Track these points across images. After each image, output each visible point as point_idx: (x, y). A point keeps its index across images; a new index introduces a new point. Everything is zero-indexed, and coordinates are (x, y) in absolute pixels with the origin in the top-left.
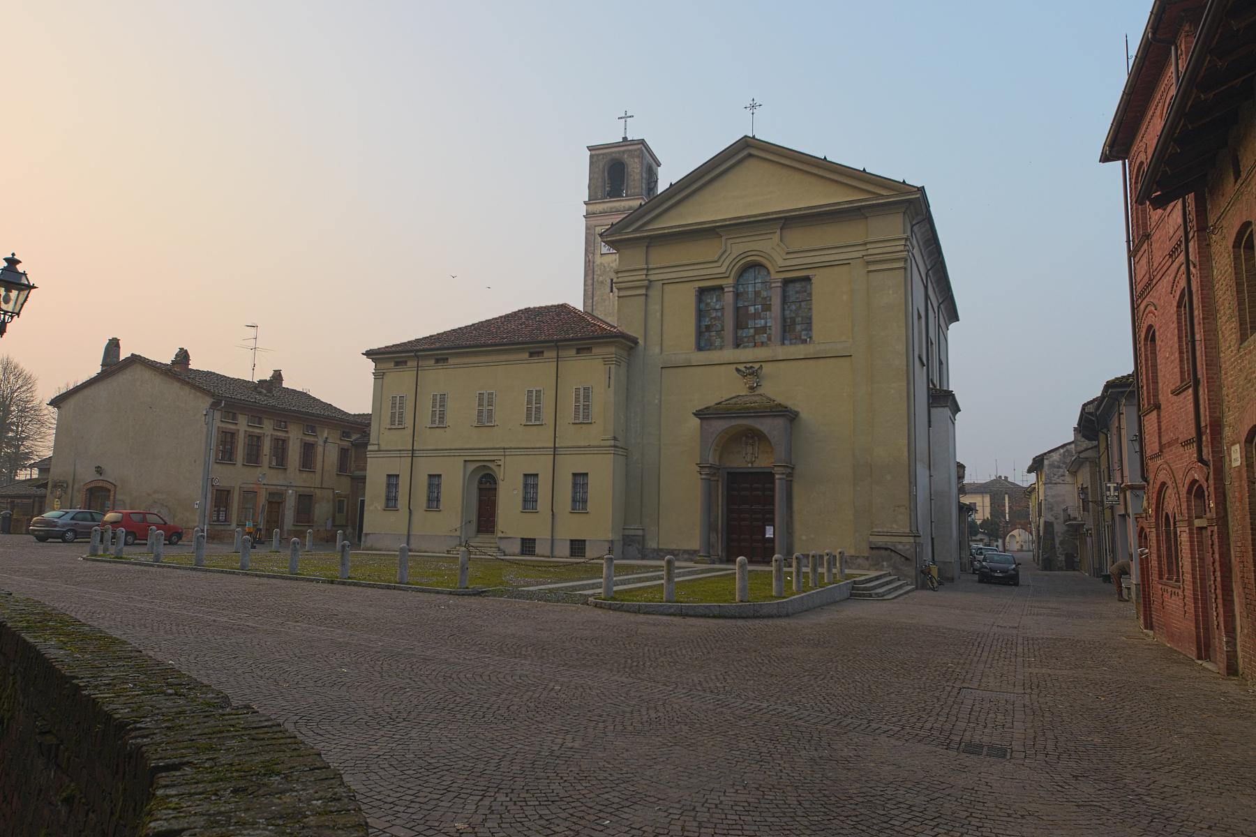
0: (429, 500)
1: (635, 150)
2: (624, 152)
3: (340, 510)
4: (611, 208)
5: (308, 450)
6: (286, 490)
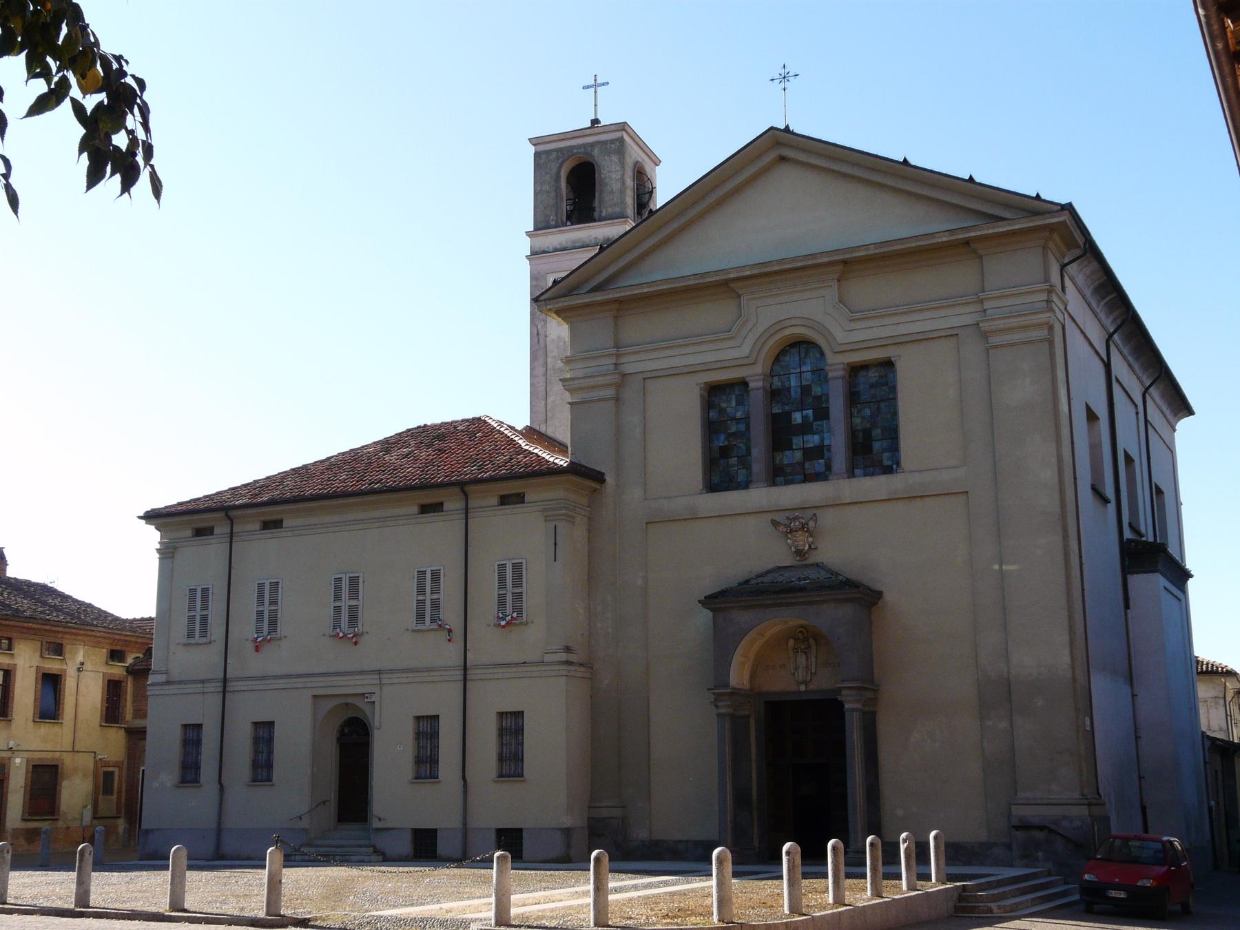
0: (255, 765)
1: (612, 141)
2: (592, 145)
3: (107, 789)
4: (574, 242)
5: (51, 682)
6: (9, 759)
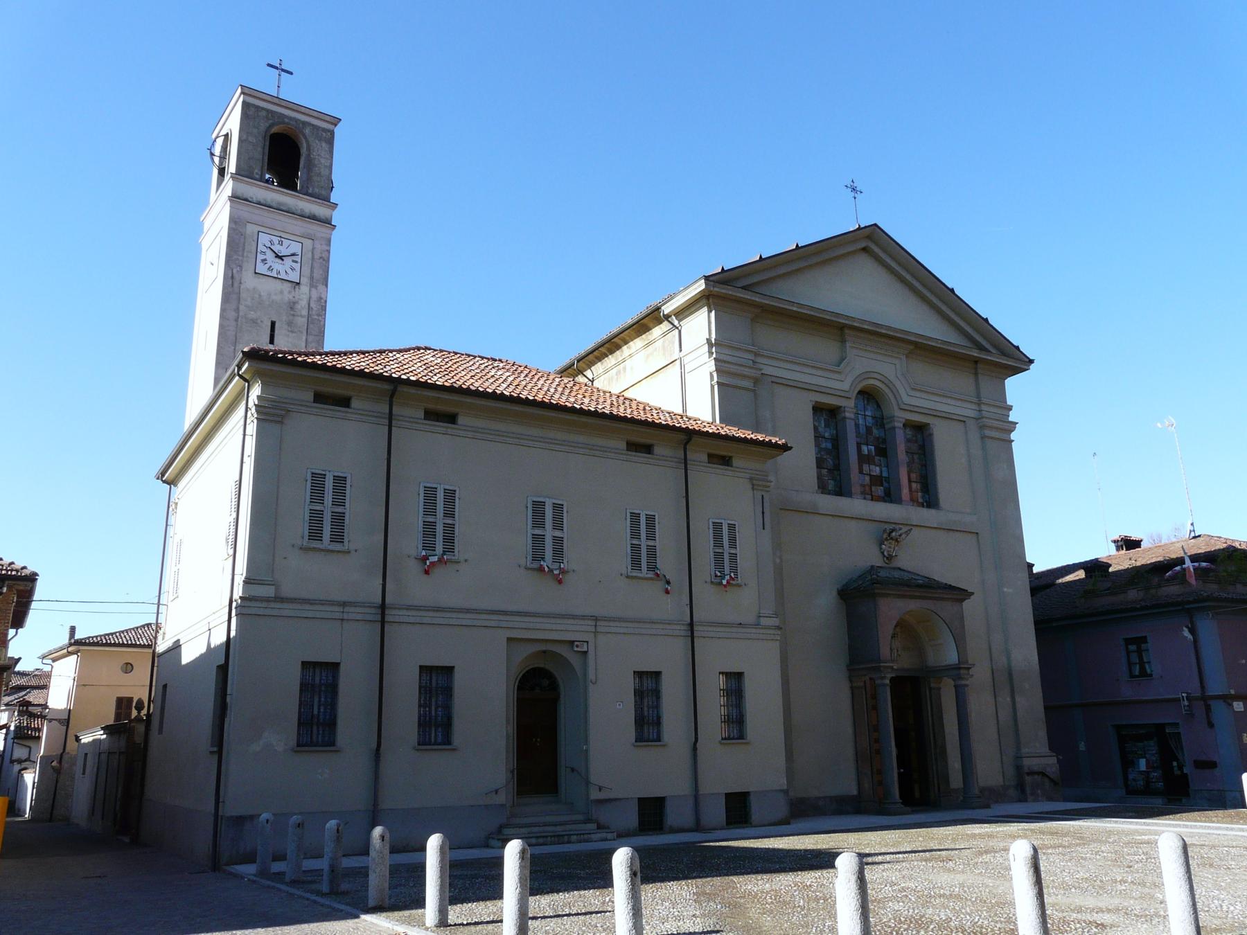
0: (424, 724)
1: (325, 130)
4: (279, 203)
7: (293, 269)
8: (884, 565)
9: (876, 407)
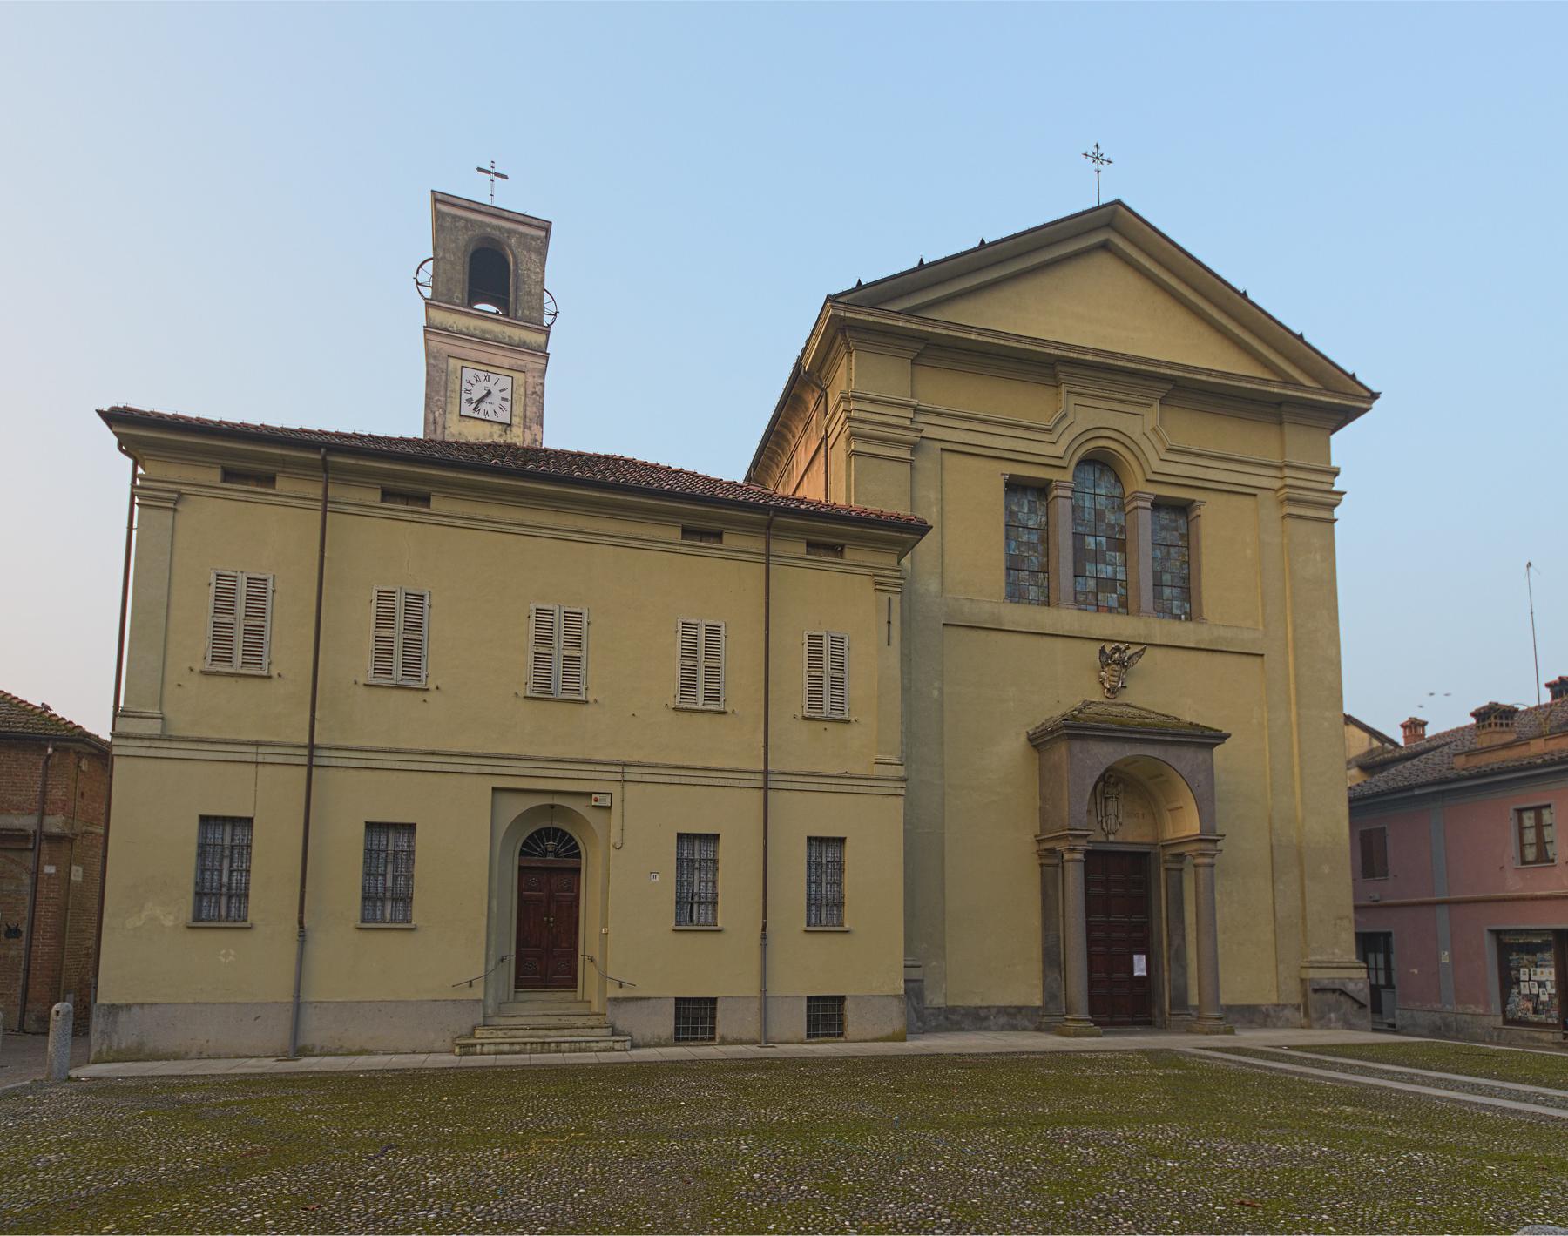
0: (369, 898)
2: (510, 232)
4: (484, 331)
7: (502, 408)
8: (1105, 700)
9: (1113, 481)
